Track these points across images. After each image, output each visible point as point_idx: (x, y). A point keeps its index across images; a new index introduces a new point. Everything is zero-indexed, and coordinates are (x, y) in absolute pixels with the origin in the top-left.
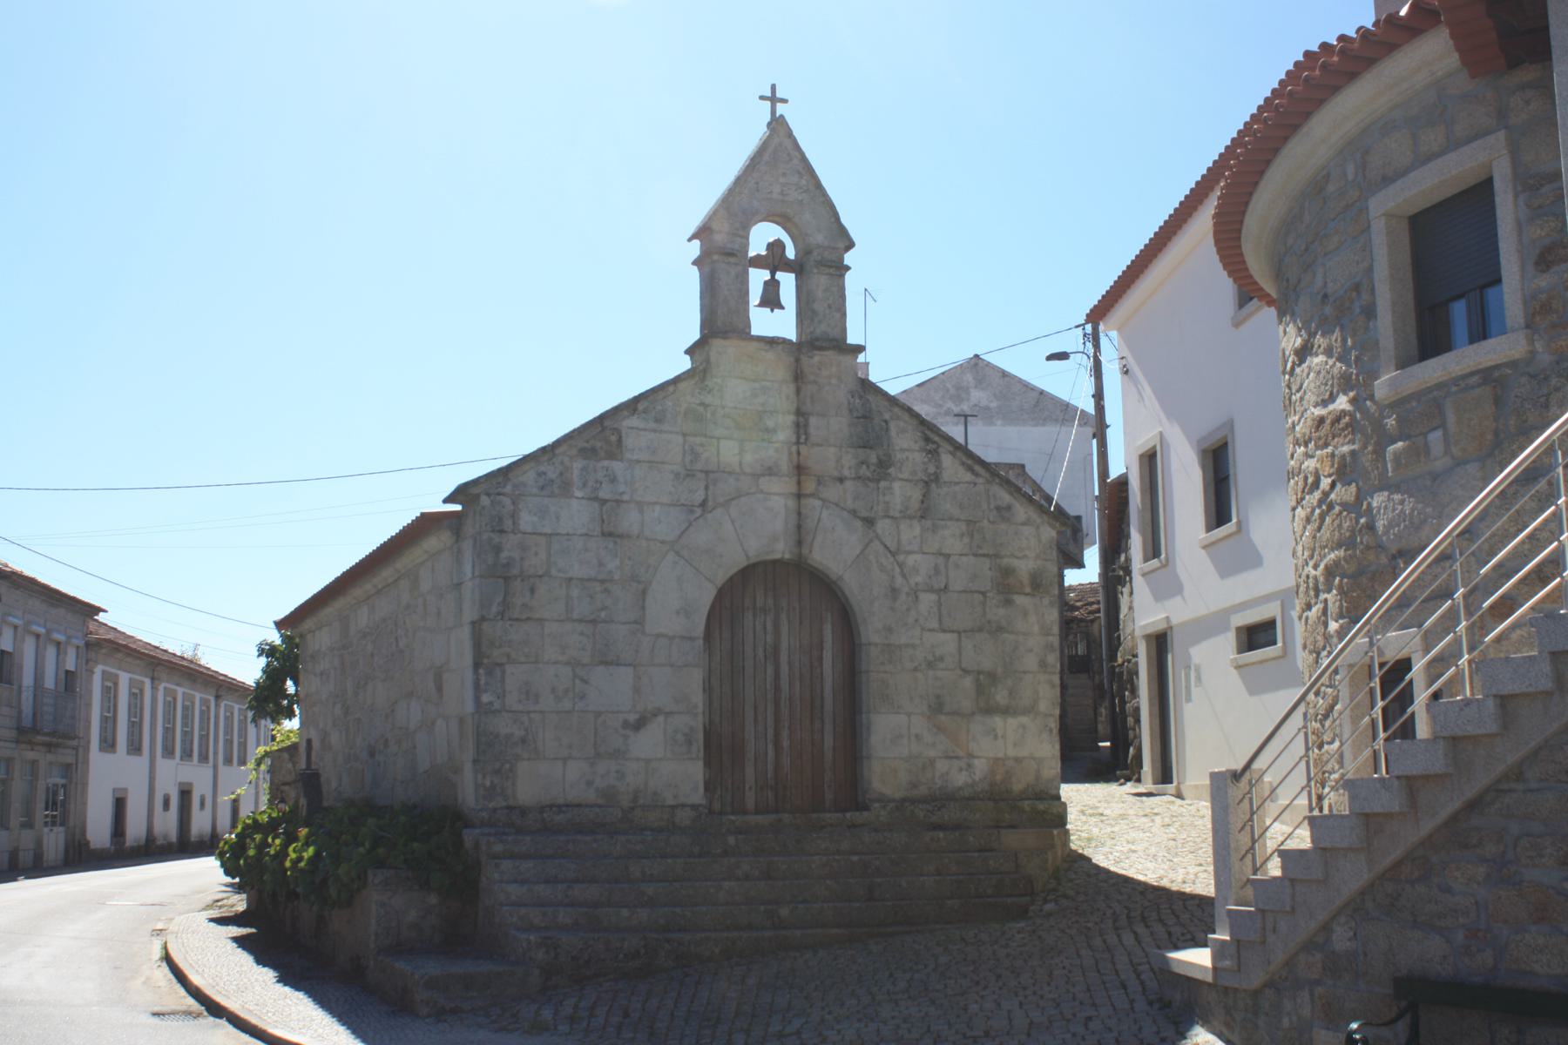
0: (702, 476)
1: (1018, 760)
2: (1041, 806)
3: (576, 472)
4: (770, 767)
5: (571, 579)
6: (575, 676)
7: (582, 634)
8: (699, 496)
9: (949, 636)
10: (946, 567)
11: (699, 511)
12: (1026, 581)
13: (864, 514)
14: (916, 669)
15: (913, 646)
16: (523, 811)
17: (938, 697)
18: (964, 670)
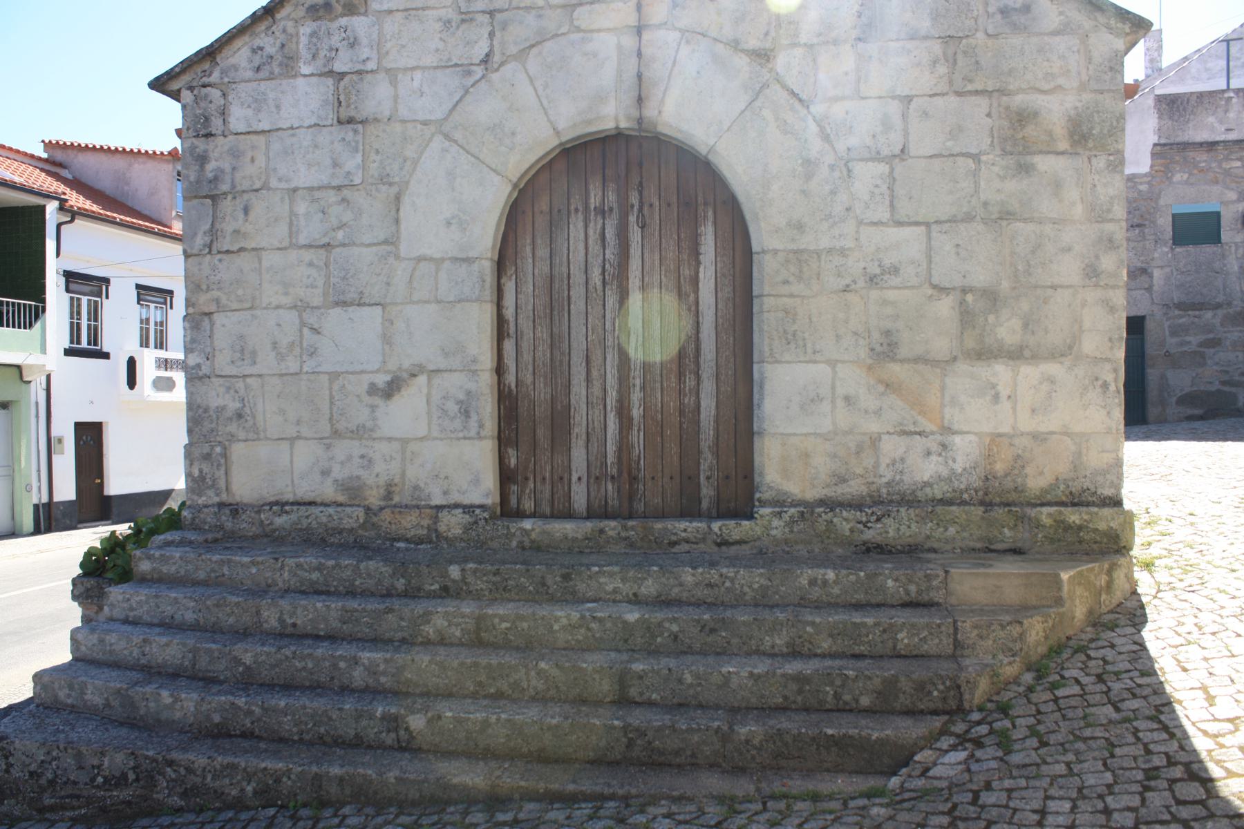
0: (485, 18)
1: (1038, 437)
2: (1074, 516)
3: (304, 40)
4: (611, 448)
5: (295, 190)
6: (303, 324)
7: (311, 264)
8: (481, 49)
9: (907, 231)
10: (904, 116)
11: (479, 71)
12: (1060, 130)
13: (753, 43)
14: (846, 289)
15: (843, 252)
16: (235, 510)
17: (888, 333)
18: (935, 287)
